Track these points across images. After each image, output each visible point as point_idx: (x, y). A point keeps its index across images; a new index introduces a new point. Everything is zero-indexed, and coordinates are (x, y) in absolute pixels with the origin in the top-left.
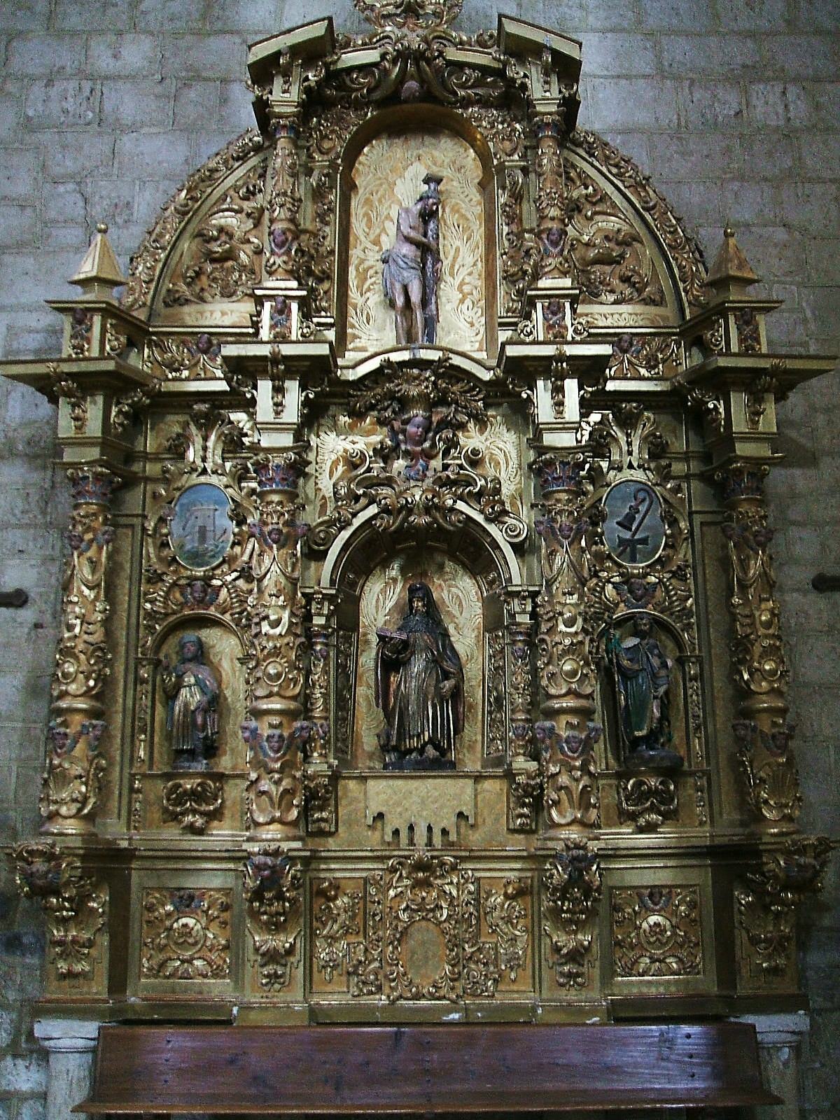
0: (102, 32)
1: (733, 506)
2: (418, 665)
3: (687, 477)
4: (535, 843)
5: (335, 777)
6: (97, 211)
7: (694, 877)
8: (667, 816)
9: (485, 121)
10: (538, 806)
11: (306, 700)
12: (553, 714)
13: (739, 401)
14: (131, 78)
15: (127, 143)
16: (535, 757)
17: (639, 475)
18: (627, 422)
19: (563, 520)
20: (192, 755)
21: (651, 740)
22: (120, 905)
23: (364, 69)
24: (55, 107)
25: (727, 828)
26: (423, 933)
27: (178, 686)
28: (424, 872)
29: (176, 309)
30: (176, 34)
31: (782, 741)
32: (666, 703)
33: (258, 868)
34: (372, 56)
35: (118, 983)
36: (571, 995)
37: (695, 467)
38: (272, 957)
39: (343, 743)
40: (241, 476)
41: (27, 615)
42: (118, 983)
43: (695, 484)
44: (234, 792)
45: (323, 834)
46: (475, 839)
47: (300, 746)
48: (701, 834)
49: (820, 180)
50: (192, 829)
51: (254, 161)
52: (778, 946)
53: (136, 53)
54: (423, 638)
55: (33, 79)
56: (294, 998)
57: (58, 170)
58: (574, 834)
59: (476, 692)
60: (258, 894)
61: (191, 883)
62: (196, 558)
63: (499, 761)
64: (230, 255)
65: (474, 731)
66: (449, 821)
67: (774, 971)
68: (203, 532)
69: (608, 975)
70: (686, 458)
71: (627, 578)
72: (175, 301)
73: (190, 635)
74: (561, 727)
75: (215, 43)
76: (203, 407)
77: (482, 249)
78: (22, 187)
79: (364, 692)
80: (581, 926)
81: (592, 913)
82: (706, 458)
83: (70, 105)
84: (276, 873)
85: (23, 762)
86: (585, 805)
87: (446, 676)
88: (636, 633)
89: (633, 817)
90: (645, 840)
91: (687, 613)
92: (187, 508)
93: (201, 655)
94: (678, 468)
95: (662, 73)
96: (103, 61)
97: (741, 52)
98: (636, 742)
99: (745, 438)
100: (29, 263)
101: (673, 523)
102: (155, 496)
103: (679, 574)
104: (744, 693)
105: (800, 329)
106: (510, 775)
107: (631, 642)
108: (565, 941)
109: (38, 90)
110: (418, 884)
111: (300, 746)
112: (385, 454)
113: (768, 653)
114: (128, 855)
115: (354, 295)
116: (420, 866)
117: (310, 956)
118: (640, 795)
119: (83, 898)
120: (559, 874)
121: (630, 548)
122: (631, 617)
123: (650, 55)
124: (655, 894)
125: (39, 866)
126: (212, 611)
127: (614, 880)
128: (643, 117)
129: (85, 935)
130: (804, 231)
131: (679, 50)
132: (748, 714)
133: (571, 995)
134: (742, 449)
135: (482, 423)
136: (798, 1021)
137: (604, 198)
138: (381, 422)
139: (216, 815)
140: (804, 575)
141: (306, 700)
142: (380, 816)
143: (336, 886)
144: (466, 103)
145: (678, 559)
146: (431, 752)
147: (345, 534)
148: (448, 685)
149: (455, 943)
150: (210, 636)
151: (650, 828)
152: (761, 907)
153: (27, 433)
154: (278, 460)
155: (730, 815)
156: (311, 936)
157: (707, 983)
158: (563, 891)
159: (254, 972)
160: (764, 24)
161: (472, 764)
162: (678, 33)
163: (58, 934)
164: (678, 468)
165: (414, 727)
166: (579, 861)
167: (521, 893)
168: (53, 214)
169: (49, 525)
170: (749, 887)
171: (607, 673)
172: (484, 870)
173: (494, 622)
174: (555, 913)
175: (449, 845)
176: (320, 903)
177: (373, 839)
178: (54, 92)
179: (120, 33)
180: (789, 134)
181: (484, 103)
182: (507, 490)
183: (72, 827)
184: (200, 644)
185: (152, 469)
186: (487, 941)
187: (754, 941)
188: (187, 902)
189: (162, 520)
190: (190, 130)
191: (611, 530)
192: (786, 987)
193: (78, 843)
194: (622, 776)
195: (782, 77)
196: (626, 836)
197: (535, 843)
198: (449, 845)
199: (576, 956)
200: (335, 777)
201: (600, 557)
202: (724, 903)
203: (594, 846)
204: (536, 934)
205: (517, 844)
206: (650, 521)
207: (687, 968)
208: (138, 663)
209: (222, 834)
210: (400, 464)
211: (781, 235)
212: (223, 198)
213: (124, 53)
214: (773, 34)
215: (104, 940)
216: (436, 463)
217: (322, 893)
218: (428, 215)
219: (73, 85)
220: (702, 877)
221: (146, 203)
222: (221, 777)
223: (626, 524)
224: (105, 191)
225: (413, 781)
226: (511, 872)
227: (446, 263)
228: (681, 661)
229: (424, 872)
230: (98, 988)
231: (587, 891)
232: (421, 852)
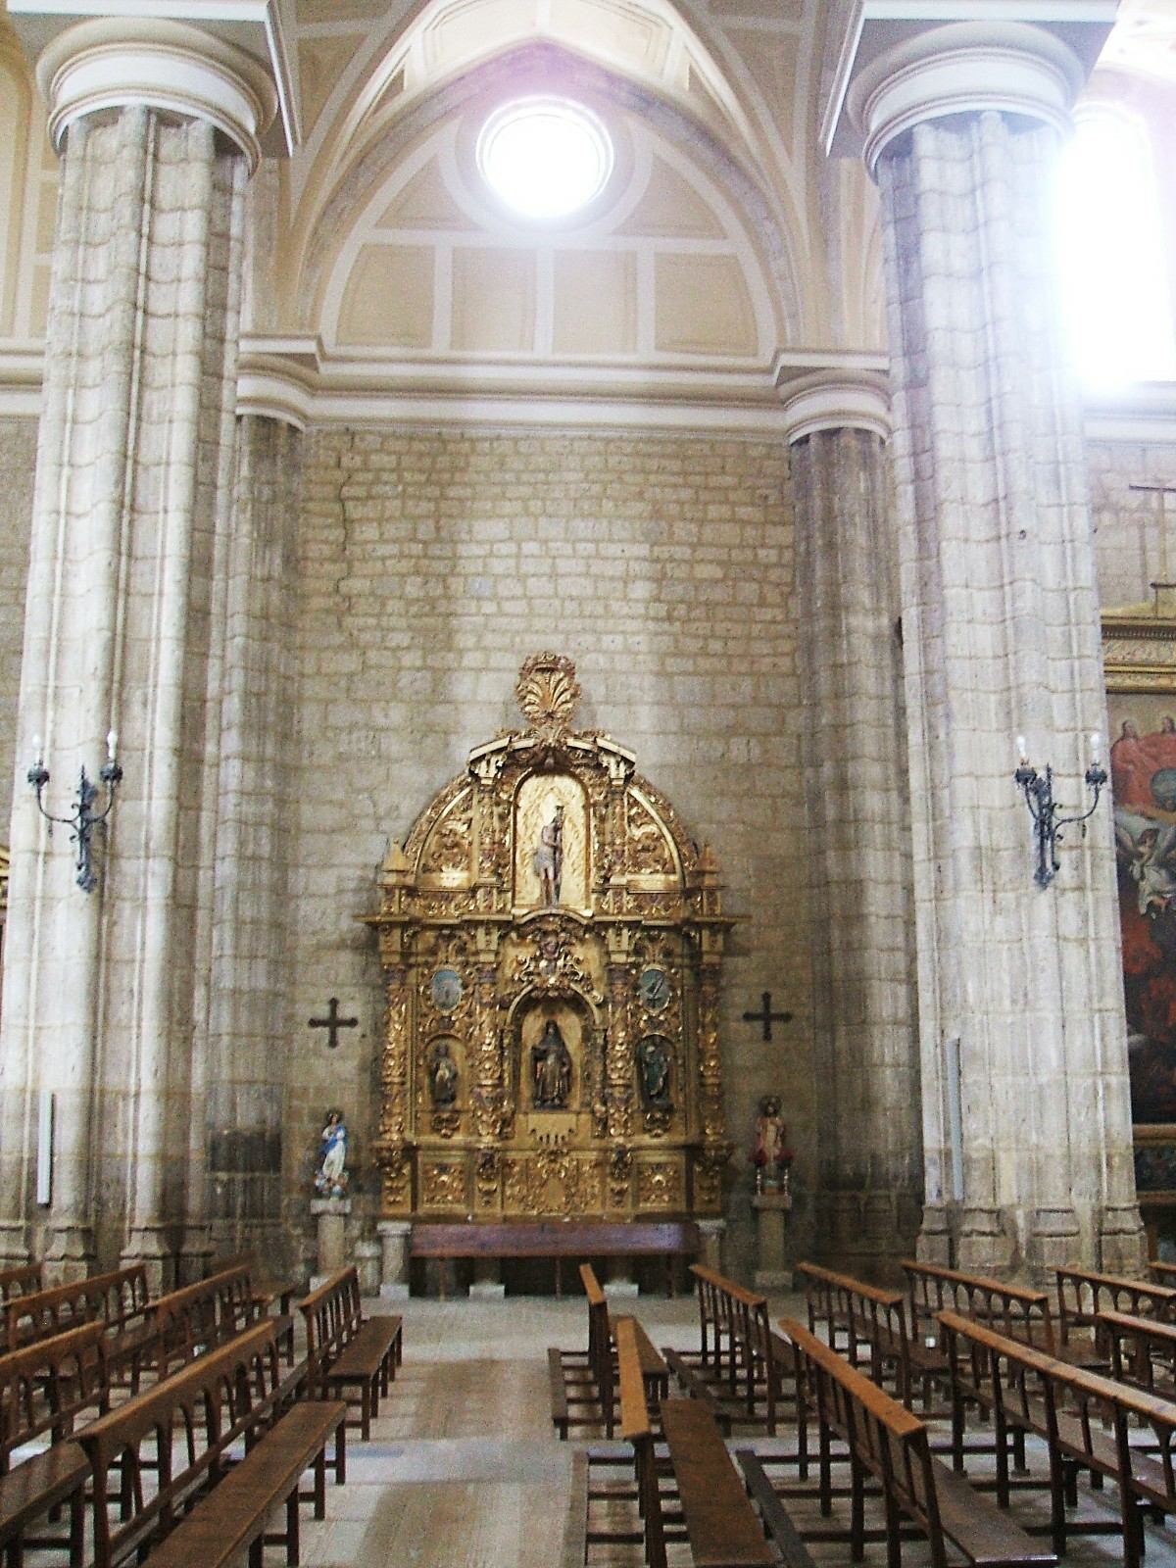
0: (378, 701)
1: (701, 986)
2: (551, 1060)
3: (681, 967)
4: (603, 1143)
5: (513, 1113)
6: (381, 811)
7: (676, 1158)
8: (666, 1130)
9: (588, 775)
10: (606, 1127)
11: (501, 1078)
12: (613, 1086)
13: (706, 933)
14: (395, 730)
15: (395, 769)
16: (604, 1104)
17: (658, 967)
18: (652, 940)
19: (619, 998)
20: (445, 1101)
21: (659, 1095)
22: (414, 1171)
23: (525, 749)
24: (354, 747)
25: (693, 1136)
26: (553, 1183)
27: (437, 1069)
28: (554, 1156)
29: (428, 875)
30: (418, 702)
31: (719, 1098)
32: (666, 1078)
33: (484, 1155)
34: (529, 743)
35: (414, 1206)
36: (618, 1210)
37: (687, 961)
38: (489, 1193)
39: (515, 1095)
40: (466, 965)
41: (358, 1030)
42: (414, 1206)
43: (687, 972)
44: (463, 1120)
45: (507, 1138)
46: (577, 1141)
47: (498, 1100)
48: (680, 1139)
49: (762, 796)
50: (445, 1136)
51: (467, 790)
52: (712, 1189)
53: (397, 714)
54: (554, 1047)
55: (341, 729)
56: (497, 1210)
57: (359, 785)
58: (621, 1140)
59: (578, 1071)
60: (483, 1166)
61: (446, 1161)
62: (444, 1006)
63: (588, 1104)
64: (456, 845)
65: (577, 1090)
66: (565, 1132)
67: (710, 1201)
68: (447, 993)
69: (635, 1204)
70: (682, 956)
71: (650, 1017)
72: (426, 869)
73: (443, 1043)
74: (617, 1093)
75: (440, 709)
76: (446, 932)
77: (583, 844)
78: (339, 795)
79: (524, 1070)
80: (622, 1180)
81: (628, 1175)
82: (692, 957)
83: (362, 745)
84: (492, 1156)
85: (361, 1103)
86: (625, 1125)
87: (564, 1064)
88: (654, 1044)
89: (650, 1131)
90: (655, 1141)
91: (677, 1034)
92: (439, 981)
93: (447, 1054)
94: (678, 961)
95: (685, 731)
96: (380, 720)
97: (729, 717)
98: (651, 1097)
99: (708, 953)
100: (346, 839)
101: (674, 989)
102: (423, 975)
103: (675, 1015)
104: (701, 1075)
105: (746, 883)
106: (593, 1112)
107: (651, 1049)
108: (484, 1186)
109: (344, 736)
110: (551, 1161)
111: (498, 1100)
112: (536, 959)
113: (712, 1057)
114: (417, 1148)
115: (518, 867)
116: (552, 1153)
117: (503, 1192)
118: (653, 1120)
119: (400, 1168)
120: (614, 1157)
121: (652, 1003)
122: (652, 1037)
123: (677, 720)
124: (659, 1167)
125: (386, 1154)
126: (452, 1032)
127: (640, 1160)
128: (671, 758)
129: (401, 1185)
130: (753, 826)
131: (694, 717)
132: (702, 1085)
133: (618, 1210)
134: (706, 958)
135: (582, 941)
136: (720, 1223)
137: (647, 814)
138: (533, 941)
139: (456, 1129)
140: (740, 1012)
141: (501, 1078)
142: (534, 1131)
143: (514, 1162)
144: (578, 766)
145: (675, 1009)
146: (557, 1101)
147: (517, 999)
148: (565, 1070)
149: (567, 1187)
150: (450, 1042)
151: (657, 1136)
152: (705, 1172)
153: (350, 936)
154: (488, 968)
155: (694, 1131)
156: (504, 1184)
157: (682, 1207)
158: (615, 1164)
159: (478, 1199)
160: (739, 700)
161: (575, 1105)
162: (693, 705)
163: (388, 1184)
164: (678, 961)
165: (549, 1090)
166: (622, 1151)
167: (596, 1165)
168: (356, 812)
169: (367, 985)
170: (700, 1163)
171: (639, 1060)
172: (581, 1155)
173: (587, 1036)
174: (612, 1174)
175: (565, 1144)
176: (507, 1170)
177: (530, 1141)
178: (354, 736)
179: (387, 702)
180: (748, 768)
181: (586, 766)
182: (594, 975)
183: (395, 1137)
184: (447, 1048)
185: (421, 959)
186: (582, 1186)
187: (701, 1188)
188: (444, 1169)
189: (427, 987)
190: (429, 762)
191: (644, 994)
192: (717, 1207)
193: (399, 1143)
194: (645, 1112)
195: (750, 734)
196: (646, 1139)
197: (603, 1143)
198: (565, 1144)
199: (621, 1193)
200: (513, 1113)
201: (638, 1007)
202: (689, 1171)
203: (629, 1146)
204: (603, 1183)
205: (596, 1143)
206: (663, 988)
207: (673, 1199)
208: (418, 1057)
209: (458, 1138)
210: (543, 964)
211: (740, 828)
212: (451, 812)
213: (391, 713)
214: (744, 706)
215: (409, 1187)
216: (560, 963)
217: (509, 1166)
218: (557, 829)
219: (363, 733)
220: (680, 1159)
221: (409, 807)
222: (458, 1112)
223: (651, 990)
224: (385, 800)
225: (604, 1455)
226: (593, 1156)
227: (565, 851)
228: (675, 1057)
229: (554, 1156)
230: (407, 1210)
231: (626, 1165)
232: (553, 1147)
